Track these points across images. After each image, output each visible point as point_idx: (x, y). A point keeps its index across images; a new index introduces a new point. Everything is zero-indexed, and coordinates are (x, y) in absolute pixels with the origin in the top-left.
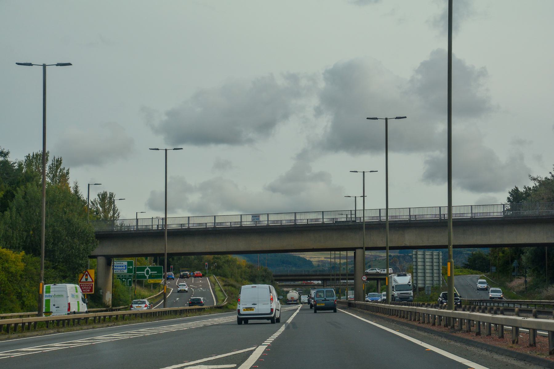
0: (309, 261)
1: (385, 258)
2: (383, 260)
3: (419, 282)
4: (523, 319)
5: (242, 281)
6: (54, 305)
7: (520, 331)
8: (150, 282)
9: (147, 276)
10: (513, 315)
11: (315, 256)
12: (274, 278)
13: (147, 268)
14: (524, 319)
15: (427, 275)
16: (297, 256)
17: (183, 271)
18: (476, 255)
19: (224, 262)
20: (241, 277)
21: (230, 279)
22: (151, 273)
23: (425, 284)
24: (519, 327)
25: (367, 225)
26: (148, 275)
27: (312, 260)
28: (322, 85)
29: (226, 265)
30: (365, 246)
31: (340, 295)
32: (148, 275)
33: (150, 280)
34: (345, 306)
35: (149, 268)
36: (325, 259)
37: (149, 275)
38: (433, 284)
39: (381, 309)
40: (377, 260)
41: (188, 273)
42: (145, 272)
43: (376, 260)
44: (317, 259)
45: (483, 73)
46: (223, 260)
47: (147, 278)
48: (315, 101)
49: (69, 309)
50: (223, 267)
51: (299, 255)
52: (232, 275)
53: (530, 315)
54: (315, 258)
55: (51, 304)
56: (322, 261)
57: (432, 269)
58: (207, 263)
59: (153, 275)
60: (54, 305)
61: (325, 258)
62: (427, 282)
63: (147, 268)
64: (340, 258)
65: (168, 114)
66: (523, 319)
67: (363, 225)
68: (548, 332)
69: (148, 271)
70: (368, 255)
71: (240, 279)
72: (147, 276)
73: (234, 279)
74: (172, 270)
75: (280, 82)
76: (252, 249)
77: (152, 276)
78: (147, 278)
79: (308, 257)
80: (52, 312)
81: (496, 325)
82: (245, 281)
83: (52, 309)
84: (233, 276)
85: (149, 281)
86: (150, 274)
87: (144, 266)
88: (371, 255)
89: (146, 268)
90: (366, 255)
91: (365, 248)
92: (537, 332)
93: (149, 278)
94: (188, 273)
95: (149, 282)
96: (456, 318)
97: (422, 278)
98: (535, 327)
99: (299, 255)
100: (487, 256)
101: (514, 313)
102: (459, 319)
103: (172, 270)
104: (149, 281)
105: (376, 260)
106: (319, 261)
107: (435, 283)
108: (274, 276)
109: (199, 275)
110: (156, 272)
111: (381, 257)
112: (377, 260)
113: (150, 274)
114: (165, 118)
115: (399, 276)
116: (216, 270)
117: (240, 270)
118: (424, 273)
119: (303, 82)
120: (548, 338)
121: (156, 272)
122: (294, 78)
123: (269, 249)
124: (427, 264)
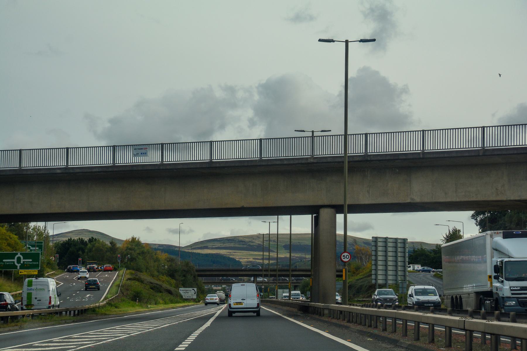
0: (239, 261)
1: (310, 260)
2: (308, 261)
3: (380, 277)
4: (423, 315)
5: (158, 276)
6: (36, 298)
7: (474, 336)
8: (22, 274)
9: (19, 265)
10: (508, 322)
11: (244, 257)
12: (197, 273)
13: (19, 255)
14: (424, 314)
15: (390, 268)
16: (227, 257)
17: (90, 264)
18: (418, 252)
19: (139, 254)
20: (158, 272)
21: (145, 273)
22: (24, 262)
23: (386, 280)
24: (473, 331)
25: (351, 162)
26: (20, 265)
27: (241, 260)
28: (256, 97)
29: (140, 257)
30: (347, 203)
31: (269, 294)
32: (20, 265)
33: (22, 271)
34: (295, 310)
35: (21, 254)
36: (254, 260)
37: (21, 264)
38: (396, 280)
39: (337, 312)
40: (303, 261)
41: (96, 266)
42: (15, 260)
43: (301, 261)
44: (246, 260)
45: (405, 90)
46: (138, 252)
47: (18, 268)
48: (250, 113)
49: (50, 303)
50: (137, 259)
51: (229, 256)
52: (147, 268)
53: (493, 318)
54: (244, 258)
55: (33, 297)
56: (251, 262)
57: (396, 261)
58: (119, 255)
59: (26, 264)
60: (36, 298)
61: (253, 259)
62: (390, 278)
63: (19, 255)
64: (269, 259)
65: (111, 121)
66: (423, 315)
67: (343, 162)
68: (520, 340)
69: (19, 259)
70: (293, 256)
71: (156, 273)
72: (19, 265)
73: (149, 273)
74: (80, 263)
75: (219, 94)
76: (133, 209)
77: (25, 266)
78: (18, 268)
79: (237, 257)
80: (33, 305)
81: (484, 333)
82: (162, 276)
83: (34, 302)
84: (148, 271)
85: (21, 272)
86: (22, 262)
87: (14, 252)
88: (297, 257)
89: (17, 254)
90: (292, 256)
91: (348, 205)
92: (419, 326)
93: (21, 267)
94: (96, 266)
95: (20, 274)
96: (380, 317)
97: (384, 272)
98: (433, 322)
99: (229, 256)
100: (431, 253)
101: (383, 308)
102: (431, 325)
103: (80, 263)
104: (21, 272)
105: (301, 261)
106: (248, 262)
107: (400, 279)
108: (197, 271)
109: (108, 268)
110: (31, 260)
111: (305, 258)
112: (303, 261)
113: (22, 262)
114: (108, 125)
115: (505, 236)
116: (129, 262)
117: (156, 263)
118: (386, 265)
119: (240, 94)
120: (520, 347)
121: (31, 260)
122: (231, 90)
123: (163, 208)
124: (390, 254)
